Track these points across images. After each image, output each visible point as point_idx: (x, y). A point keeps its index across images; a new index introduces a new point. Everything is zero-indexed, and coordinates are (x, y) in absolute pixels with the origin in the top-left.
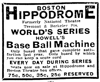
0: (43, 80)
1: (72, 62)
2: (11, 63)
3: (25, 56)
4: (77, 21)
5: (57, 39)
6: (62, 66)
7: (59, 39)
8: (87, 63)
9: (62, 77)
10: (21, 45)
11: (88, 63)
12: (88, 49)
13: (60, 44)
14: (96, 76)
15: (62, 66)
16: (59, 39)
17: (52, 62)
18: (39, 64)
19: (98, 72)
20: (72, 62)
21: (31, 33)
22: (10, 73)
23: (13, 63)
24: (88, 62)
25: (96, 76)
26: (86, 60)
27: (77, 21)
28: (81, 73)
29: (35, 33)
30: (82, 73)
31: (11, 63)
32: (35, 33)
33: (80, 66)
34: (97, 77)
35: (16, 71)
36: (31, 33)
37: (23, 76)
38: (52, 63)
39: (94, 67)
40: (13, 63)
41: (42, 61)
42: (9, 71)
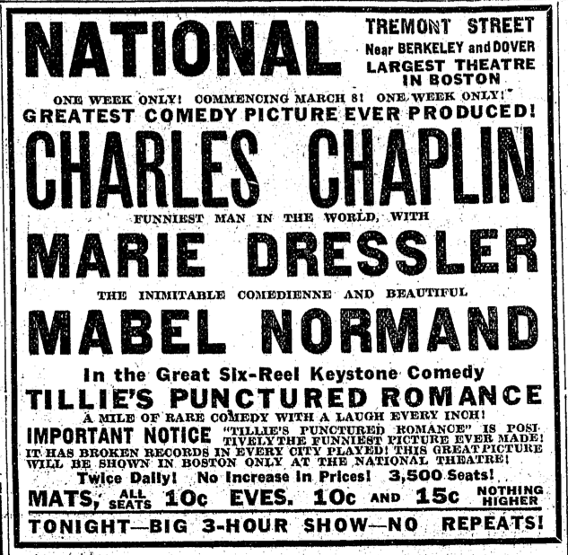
0: (186, 548)
2: (351, 116)
6: (474, 416)
8: (529, 70)
9: (78, 399)
12: (473, 472)
14: (554, 535)
15: (474, 416)
16: (334, 69)
17: (477, 113)
18: (444, 62)
19: (339, 7)
22: (237, 486)
23: (356, 114)
25: (15, 17)
31: (351, 116)
34: (11, 16)
35: (258, 417)
37: (184, 522)
38: (474, 115)
40: (356, 114)
42: (190, 465)
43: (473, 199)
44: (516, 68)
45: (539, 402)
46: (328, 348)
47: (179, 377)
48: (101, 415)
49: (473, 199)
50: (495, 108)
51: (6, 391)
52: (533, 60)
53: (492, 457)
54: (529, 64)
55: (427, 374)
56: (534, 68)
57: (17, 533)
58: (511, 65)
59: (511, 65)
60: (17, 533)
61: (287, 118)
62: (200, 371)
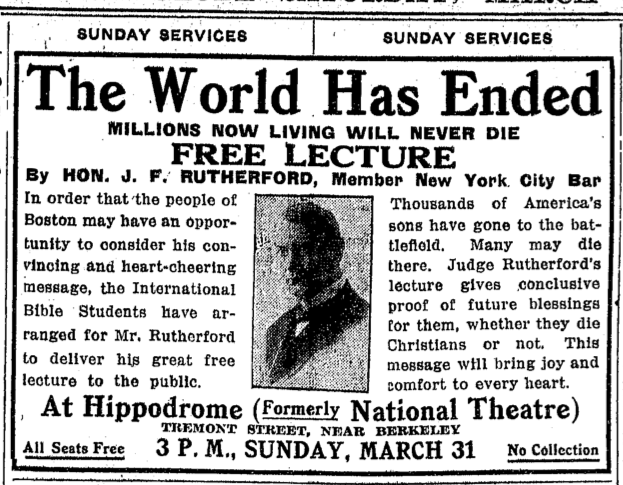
1: (246, 454)
3: (247, 418)
4: (151, 265)
5: (391, 137)
7: (397, 137)
10: (402, 94)
11: (525, 180)
13: (170, 90)
16: (397, 137)
20: (246, 454)
21: (426, 159)
24: (513, 180)
26: (511, 129)
27: (151, 265)
28: (497, 35)
29: (381, 134)
30: (500, 36)
32: (381, 134)
33: (217, 407)
36: (426, 159)
39: (74, 339)
41: (449, 35)
43: (152, 134)
44: (223, 181)
45: (517, 138)
46: (202, 95)
47: (507, 306)
48: (473, 241)
49: (152, 134)
50: (221, 33)
51: (574, 180)
52: (517, 128)
53: (213, 149)
54: (438, 443)
55: (483, 182)
56: (257, 127)
57: (14, 461)
58: (218, 177)
59: (218, 177)
60: (14, 461)
61: (213, 180)
62: (532, 404)
